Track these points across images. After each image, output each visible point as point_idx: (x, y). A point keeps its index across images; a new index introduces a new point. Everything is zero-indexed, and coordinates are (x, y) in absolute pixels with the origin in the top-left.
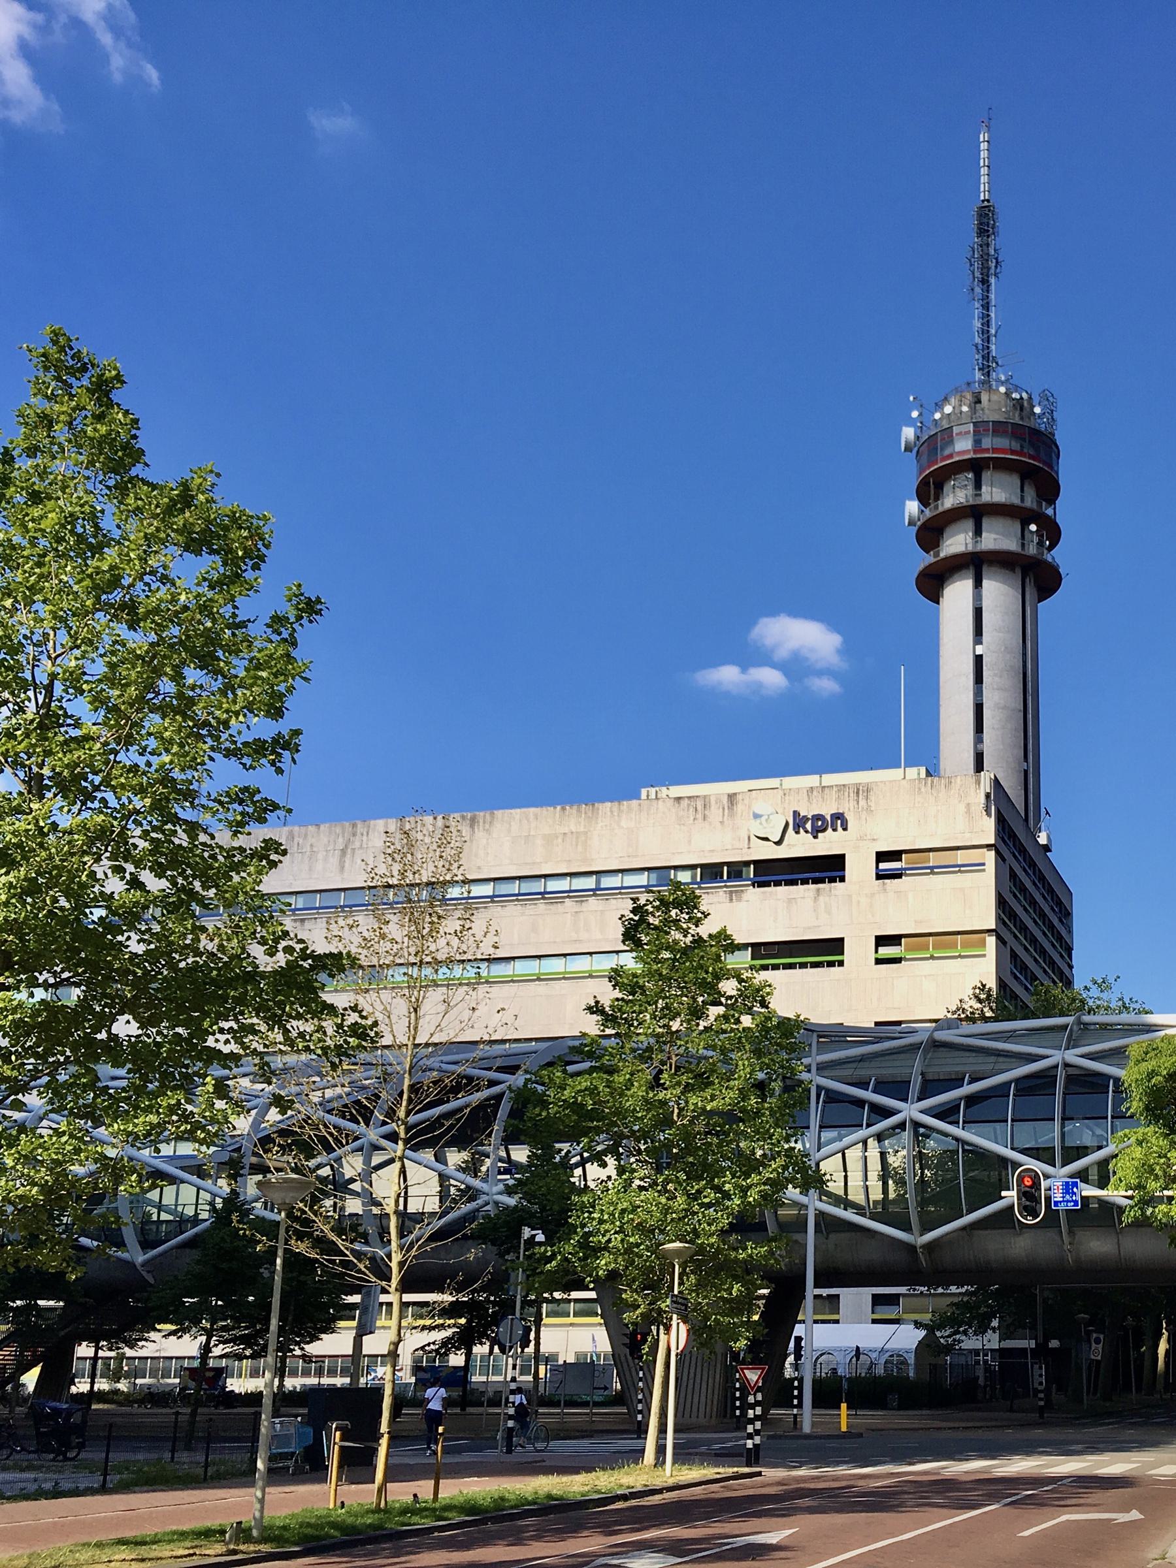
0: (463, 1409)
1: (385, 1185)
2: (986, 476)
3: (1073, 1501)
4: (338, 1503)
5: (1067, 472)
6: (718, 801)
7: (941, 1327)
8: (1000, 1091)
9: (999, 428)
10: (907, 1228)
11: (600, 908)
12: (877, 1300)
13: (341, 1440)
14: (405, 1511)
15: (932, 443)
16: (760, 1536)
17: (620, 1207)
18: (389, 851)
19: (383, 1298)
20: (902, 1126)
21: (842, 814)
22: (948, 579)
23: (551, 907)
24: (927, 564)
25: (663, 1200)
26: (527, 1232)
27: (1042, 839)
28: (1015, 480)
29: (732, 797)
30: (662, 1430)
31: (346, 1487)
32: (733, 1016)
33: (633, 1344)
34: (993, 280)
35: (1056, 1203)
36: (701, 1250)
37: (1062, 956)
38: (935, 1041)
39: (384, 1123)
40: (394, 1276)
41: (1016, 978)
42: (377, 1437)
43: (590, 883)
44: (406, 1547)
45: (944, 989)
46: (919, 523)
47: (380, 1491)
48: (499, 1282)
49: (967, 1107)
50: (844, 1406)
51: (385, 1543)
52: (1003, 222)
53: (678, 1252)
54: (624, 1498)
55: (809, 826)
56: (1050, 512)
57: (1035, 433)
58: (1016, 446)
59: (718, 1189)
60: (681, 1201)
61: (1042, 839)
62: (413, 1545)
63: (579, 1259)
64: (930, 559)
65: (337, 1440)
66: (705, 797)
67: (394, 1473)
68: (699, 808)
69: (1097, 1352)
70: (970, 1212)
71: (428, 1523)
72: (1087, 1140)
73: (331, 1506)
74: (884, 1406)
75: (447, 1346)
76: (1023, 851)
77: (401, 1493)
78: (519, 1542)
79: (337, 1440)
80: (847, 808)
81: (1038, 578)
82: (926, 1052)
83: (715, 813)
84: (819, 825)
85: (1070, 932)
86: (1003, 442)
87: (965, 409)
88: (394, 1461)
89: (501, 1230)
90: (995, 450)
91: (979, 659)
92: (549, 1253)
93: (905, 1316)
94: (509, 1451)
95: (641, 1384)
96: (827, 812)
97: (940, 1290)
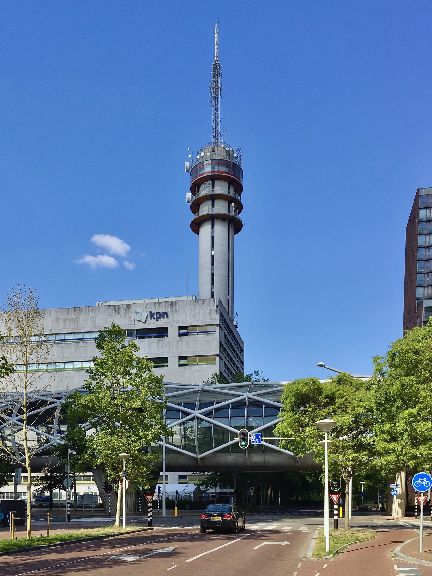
0: (51, 509)
1: (20, 436)
2: (216, 183)
3: (266, 538)
4: (15, 538)
5: (246, 182)
6: (123, 307)
7: (202, 485)
8: (226, 407)
9: (221, 162)
10: (195, 452)
11: (84, 345)
12: (180, 477)
13: (14, 517)
14: (39, 540)
15: (196, 169)
16: (183, 550)
17: (104, 440)
18: (9, 302)
19: (23, 474)
20: (192, 419)
21: (167, 312)
22: (202, 224)
23: (67, 345)
24: (194, 218)
25: (118, 439)
26: (70, 451)
27: (235, 324)
28: (226, 185)
29: (128, 305)
30: (121, 515)
31: (16, 532)
32: (139, 374)
33: (108, 489)
34: (219, 98)
35: (253, 442)
36: (132, 456)
37: (240, 365)
38: (204, 390)
39: (17, 416)
40: (27, 461)
41: (226, 372)
42: (26, 516)
43: (79, 336)
44: (41, 552)
45: (201, 376)
46: (191, 202)
47: (29, 533)
48: (61, 469)
49: (215, 412)
50: (176, 508)
51: (33, 551)
52: (222, 71)
53: (124, 457)
54: (111, 536)
55: (155, 317)
56: (239, 198)
57: (234, 165)
58: (227, 170)
59: (137, 435)
60: (124, 439)
61: (235, 324)
62: (43, 552)
63: (90, 459)
64: (195, 217)
65: (12, 517)
66: (118, 305)
67: (33, 528)
68: (117, 309)
69: (251, 492)
70: (215, 447)
71: (46, 544)
72: (254, 424)
73: (12, 538)
74: (185, 509)
75: (43, 490)
76: (229, 327)
77: (36, 534)
78: (81, 551)
79: (12, 517)
80: (168, 310)
81: (235, 226)
82: (201, 393)
83: (122, 312)
84: (159, 316)
85: (243, 357)
86: (222, 169)
87: (208, 154)
88: (32, 524)
89: (62, 451)
90: (220, 172)
91: (213, 257)
92: (80, 457)
93: (189, 482)
94: (69, 521)
95: (109, 501)
96: (162, 311)
97: (202, 474)
